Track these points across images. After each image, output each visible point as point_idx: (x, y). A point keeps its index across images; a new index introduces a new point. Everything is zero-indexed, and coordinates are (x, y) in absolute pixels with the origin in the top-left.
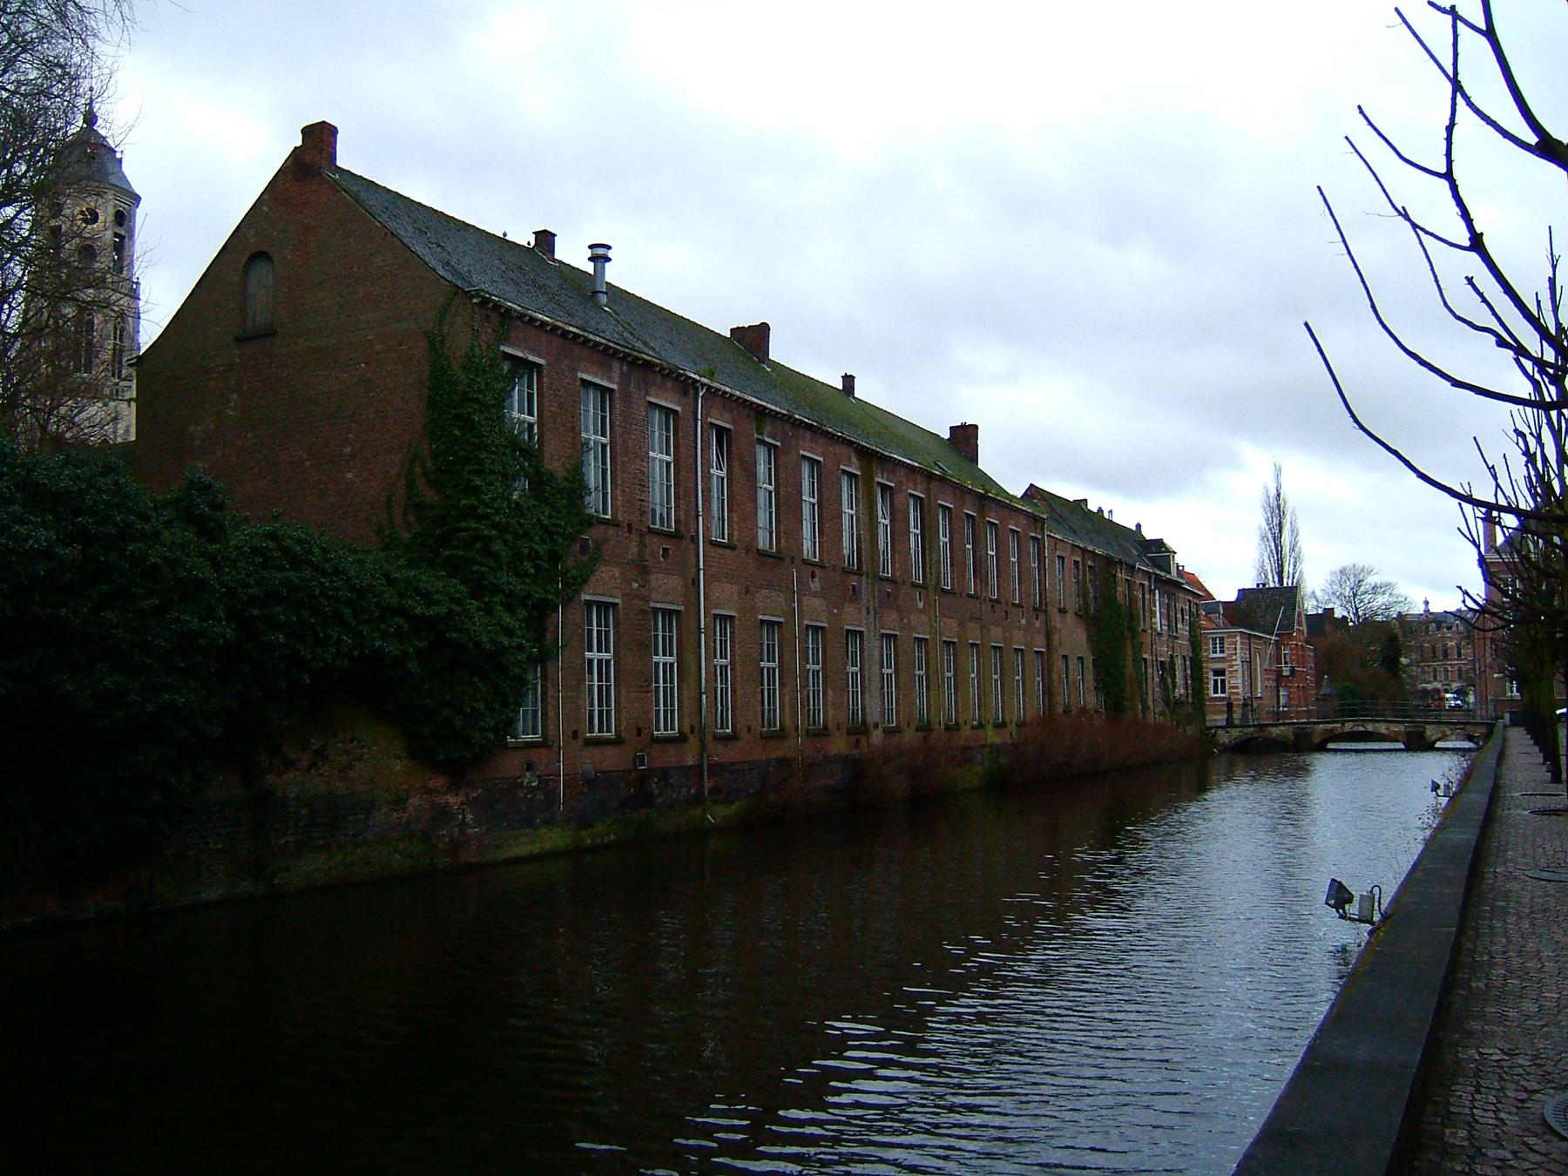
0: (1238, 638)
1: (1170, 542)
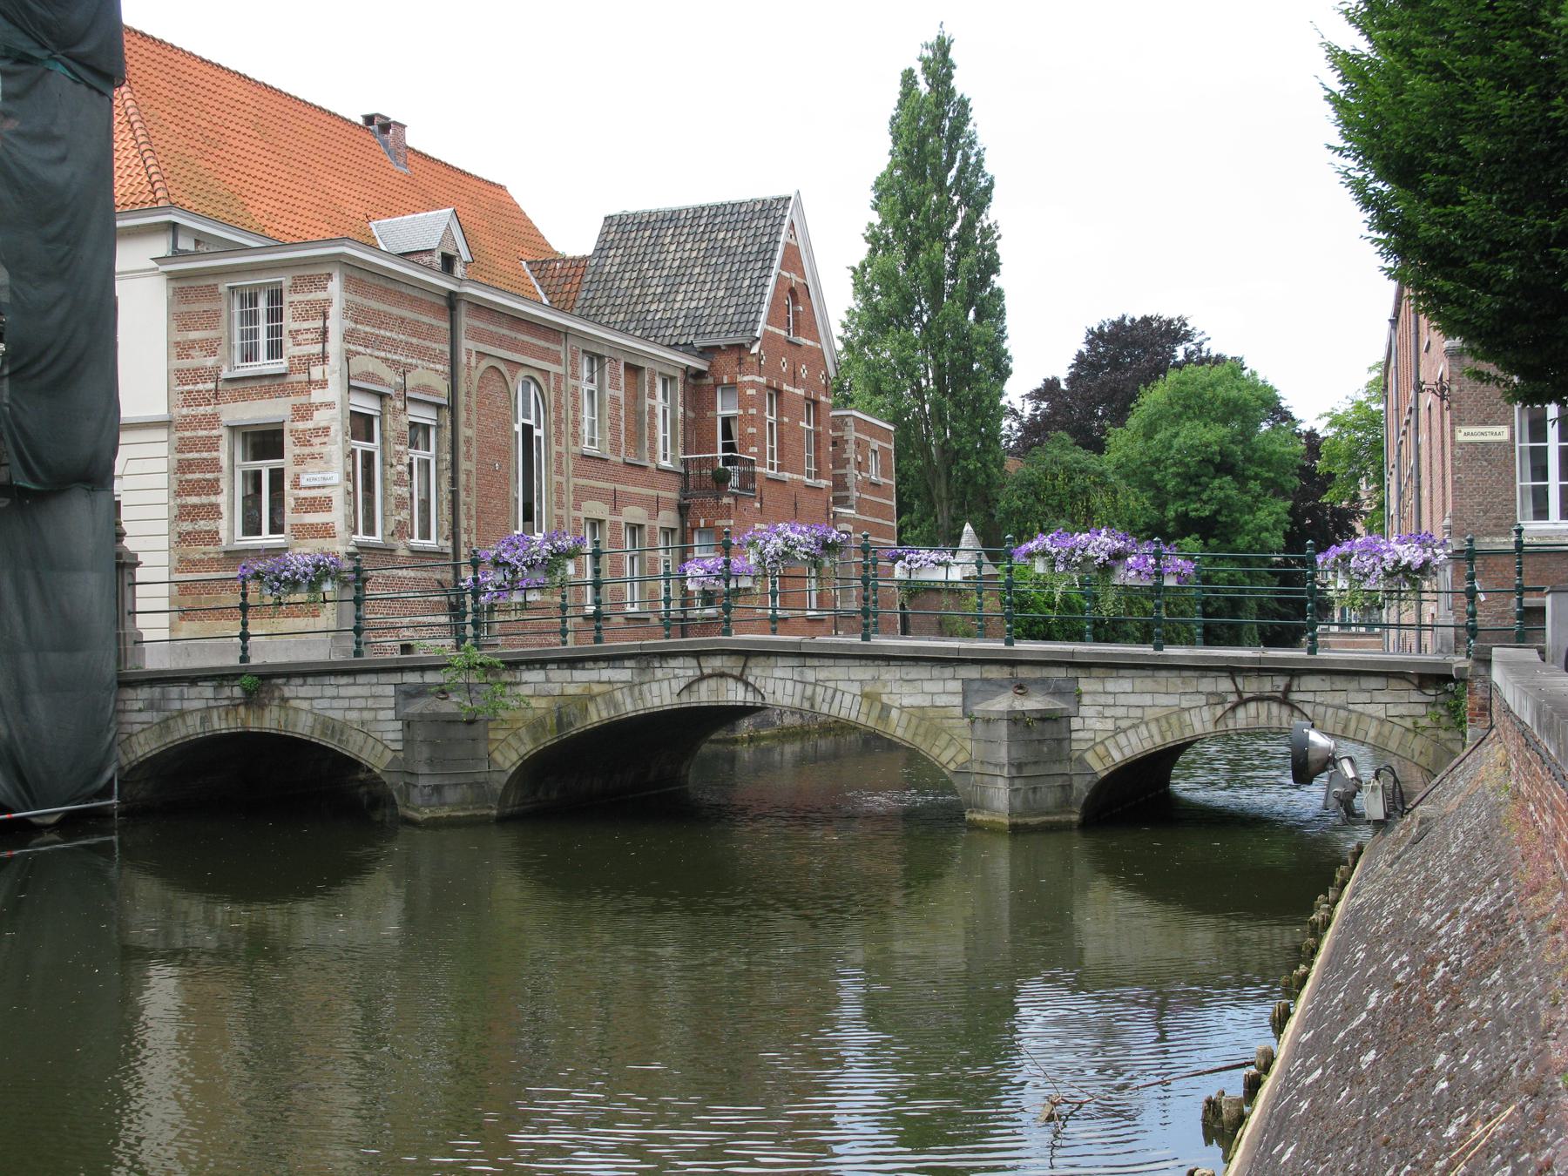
0: (335, 288)
1: (1105, 313)
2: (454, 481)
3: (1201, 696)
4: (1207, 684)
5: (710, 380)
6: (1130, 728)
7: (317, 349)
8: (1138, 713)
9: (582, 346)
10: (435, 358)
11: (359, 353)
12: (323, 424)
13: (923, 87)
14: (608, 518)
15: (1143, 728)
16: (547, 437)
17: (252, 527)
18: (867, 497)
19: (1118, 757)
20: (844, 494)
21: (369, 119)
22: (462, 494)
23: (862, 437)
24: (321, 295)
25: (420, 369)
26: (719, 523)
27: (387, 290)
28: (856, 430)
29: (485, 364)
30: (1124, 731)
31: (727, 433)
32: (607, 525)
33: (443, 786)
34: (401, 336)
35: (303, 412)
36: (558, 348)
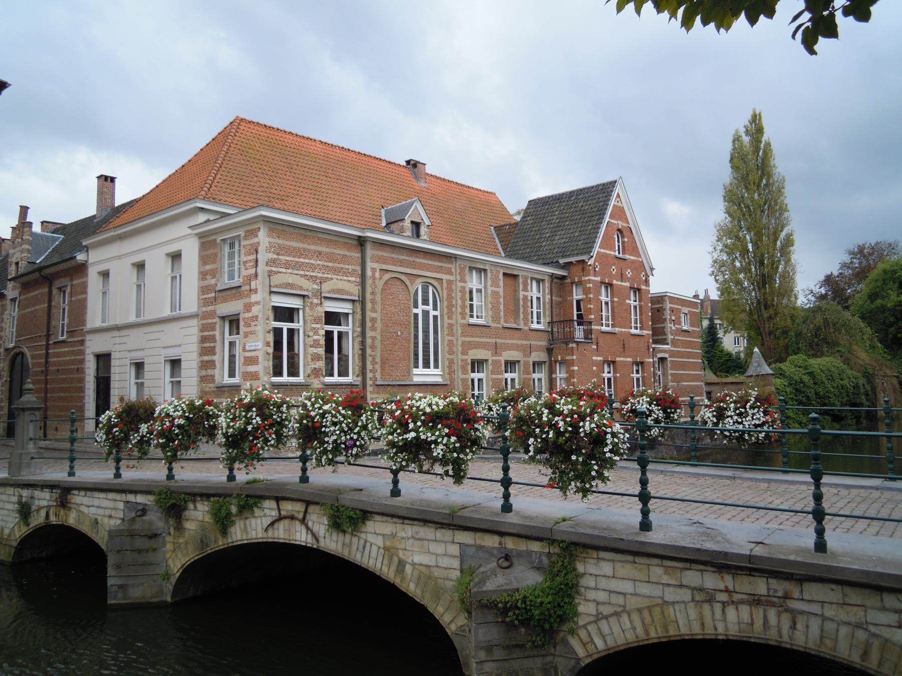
2: (363, 343)
3: (684, 590)
4: (692, 577)
5: (569, 281)
6: (612, 615)
7: (253, 271)
8: (620, 600)
9: (468, 264)
10: (352, 274)
11: (280, 273)
12: (256, 314)
13: (746, 139)
14: (491, 359)
15: (625, 618)
16: (442, 315)
17: (278, 372)
18: (680, 338)
19: (600, 645)
20: (664, 337)
21: (408, 162)
22: (369, 351)
23: (676, 306)
24: (255, 240)
25: (335, 280)
26: (568, 358)
27: (306, 236)
28: (670, 303)
29: (387, 276)
30: (606, 618)
31: (579, 309)
32: (490, 362)
33: (127, 585)
34: (319, 262)
35: (248, 307)
36: (450, 266)
